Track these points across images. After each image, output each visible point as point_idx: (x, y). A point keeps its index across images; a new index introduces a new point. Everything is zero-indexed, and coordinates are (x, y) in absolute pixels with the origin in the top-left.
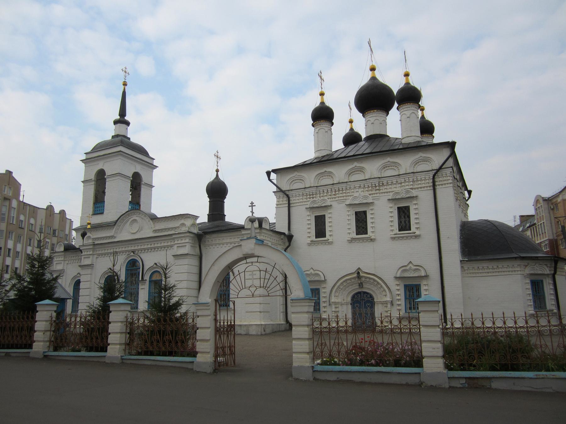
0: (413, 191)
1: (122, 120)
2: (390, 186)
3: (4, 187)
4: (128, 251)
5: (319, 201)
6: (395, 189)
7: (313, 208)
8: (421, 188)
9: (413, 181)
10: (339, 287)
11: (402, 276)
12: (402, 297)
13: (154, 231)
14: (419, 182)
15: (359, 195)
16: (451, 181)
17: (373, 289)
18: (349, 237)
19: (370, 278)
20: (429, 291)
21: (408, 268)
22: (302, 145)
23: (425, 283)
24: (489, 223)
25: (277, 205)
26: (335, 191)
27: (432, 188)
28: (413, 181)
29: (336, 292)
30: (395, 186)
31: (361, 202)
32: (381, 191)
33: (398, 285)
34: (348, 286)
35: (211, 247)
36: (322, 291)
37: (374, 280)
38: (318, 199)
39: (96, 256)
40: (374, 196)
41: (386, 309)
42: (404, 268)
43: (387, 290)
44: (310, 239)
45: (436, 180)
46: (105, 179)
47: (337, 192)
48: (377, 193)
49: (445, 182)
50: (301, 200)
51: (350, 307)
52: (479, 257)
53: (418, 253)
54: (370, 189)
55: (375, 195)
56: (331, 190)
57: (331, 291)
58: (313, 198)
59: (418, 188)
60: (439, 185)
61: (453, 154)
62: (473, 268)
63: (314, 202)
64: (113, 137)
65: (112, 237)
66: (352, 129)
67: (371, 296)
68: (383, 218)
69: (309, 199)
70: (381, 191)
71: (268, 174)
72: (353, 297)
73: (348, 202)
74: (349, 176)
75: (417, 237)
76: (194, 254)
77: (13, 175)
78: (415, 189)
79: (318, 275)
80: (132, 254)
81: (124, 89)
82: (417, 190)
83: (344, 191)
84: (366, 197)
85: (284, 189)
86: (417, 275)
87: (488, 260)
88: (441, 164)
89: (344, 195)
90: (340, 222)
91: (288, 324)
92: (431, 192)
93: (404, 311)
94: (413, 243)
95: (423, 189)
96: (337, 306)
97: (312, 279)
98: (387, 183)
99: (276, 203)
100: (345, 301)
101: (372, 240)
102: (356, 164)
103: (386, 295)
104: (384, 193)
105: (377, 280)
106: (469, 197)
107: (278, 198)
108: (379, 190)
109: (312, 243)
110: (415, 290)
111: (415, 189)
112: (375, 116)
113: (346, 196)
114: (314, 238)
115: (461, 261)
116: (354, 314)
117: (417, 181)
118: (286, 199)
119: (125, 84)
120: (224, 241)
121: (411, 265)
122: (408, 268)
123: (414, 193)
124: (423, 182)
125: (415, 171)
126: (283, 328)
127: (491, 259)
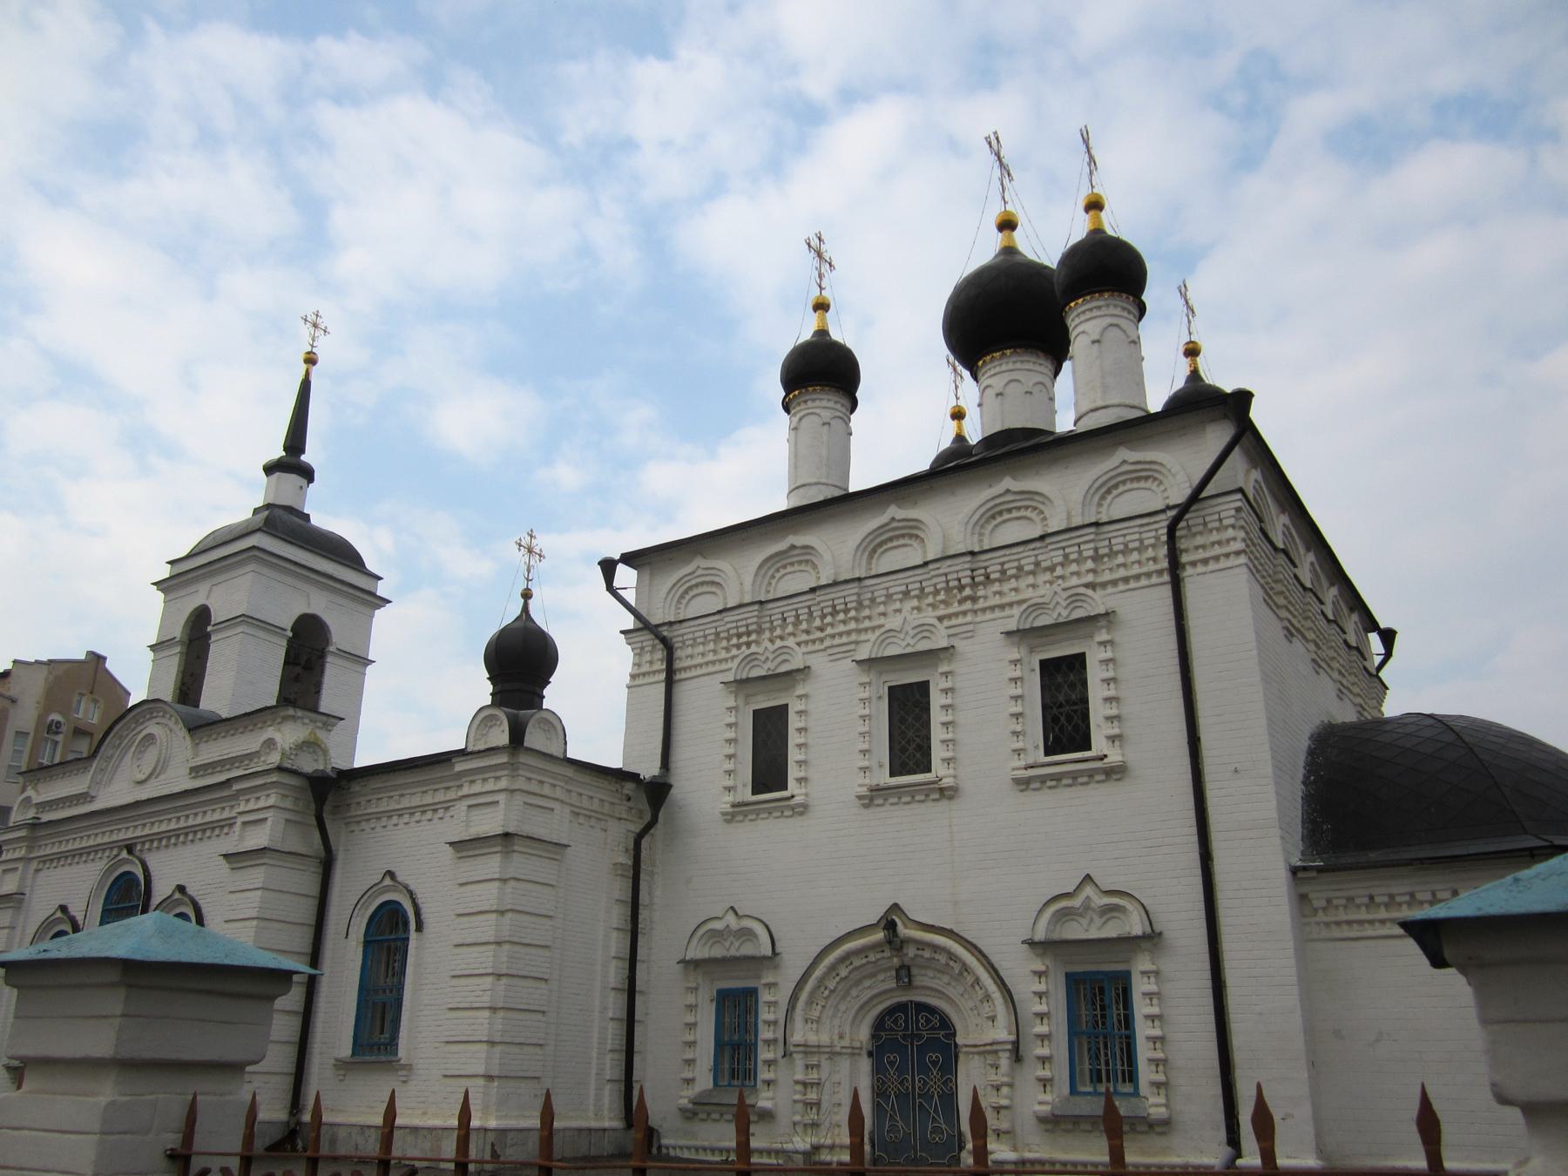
0: (1097, 595)
1: (292, 463)
2: (1013, 583)
3: (76, 698)
4: (110, 846)
5: (768, 655)
6: (1029, 593)
7: (748, 680)
8: (1126, 580)
9: (1097, 558)
10: (821, 982)
11: (1056, 936)
12: (1059, 1026)
13: (192, 769)
14: (1120, 559)
15: (903, 625)
16: (1239, 546)
17: (950, 991)
18: (860, 784)
19: (936, 948)
20: (1170, 1010)
21: (1076, 902)
22: (750, 470)
23: (1148, 966)
24: (1450, 738)
25: (633, 677)
26: (823, 616)
27: (1166, 577)
28: (1097, 558)
29: (810, 1002)
30: (1030, 580)
31: (909, 650)
32: (981, 604)
33: (1039, 974)
34: (858, 982)
35: (364, 825)
36: (765, 996)
37: (952, 956)
38: (765, 646)
39: (34, 865)
40: (954, 622)
41: (993, 1077)
42: (1062, 905)
43: (997, 995)
44: (729, 798)
45: (1182, 544)
46: (208, 636)
47: (829, 619)
48: (964, 613)
49: (1217, 550)
50: (711, 657)
51: (865, 1065)
52: (1373, 856)
53: (1117, 840)
54: (942, 596)
55: (960, 620)
56: (810, 613)
57: (794, 997)
58: (748, 644)
59: (1114, 583)
60: (1194, 564)
61: (1248, 438)
62: (1350, 899)
63: (751, 659)
64: (256, 511)
65: (84, 797)
66: (1194, 375)
67: (946, 1025)
68: (985, 709)
69: (734, 652)
70: (981, 604)
71: (608, 567)
72: (879, 1025)
73: (863, 653)
74: (871, 557)
75: (1115, 773)
76: (302, 850)
77: (108, 665)
78: (1104, 585)
79: (747, 934)
80: (124, 854)
81: (308, 373)
82: (1110, 590)
83: (853, 613)
84: (923, 630)
85: (654, 620)
86: (1113, 934)
87: (1409, 863)
88: (1196, 480)
89: (853, 625)
90: (838, 728)
91: (637, 1134)
92: (1166, 593)
93: (1066, 1090)
94: (1098, 796)
95: (1133, 584)
96: (813, 1060)
97: (733, 952)
98: (1003, 572)
99: (630, 670)
100: (846, 1042)
101: (947, 793)
102: (893, 511)
103: (993, 1019)
104: (992, 608)
105: (958, 952)
106: (1388, 655)
107: (639, 652)
108: (974, 599)
109: (739, 811)
110: (1111, 994)
111: (1104, 585)
112: (1013, 371)
113: (859, 631)
114: (746, 794)
115: (1294, 871)
116: (879, 1092)
117: (1112, 554)
118: (660, 654)
119: (311, 360)
120: (405, 803)
121: (1089, 890)
122: (1076, 902)
123: (1098, 602)
124: (1135, 556)
125: (1105, 519)
126: (607, 1147)
127: (1421, 861)
